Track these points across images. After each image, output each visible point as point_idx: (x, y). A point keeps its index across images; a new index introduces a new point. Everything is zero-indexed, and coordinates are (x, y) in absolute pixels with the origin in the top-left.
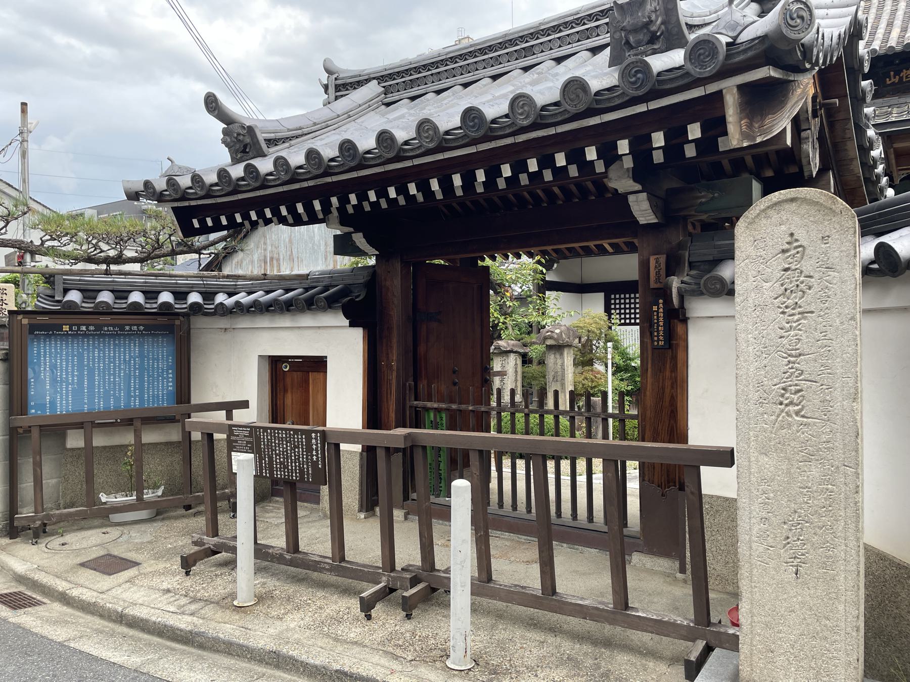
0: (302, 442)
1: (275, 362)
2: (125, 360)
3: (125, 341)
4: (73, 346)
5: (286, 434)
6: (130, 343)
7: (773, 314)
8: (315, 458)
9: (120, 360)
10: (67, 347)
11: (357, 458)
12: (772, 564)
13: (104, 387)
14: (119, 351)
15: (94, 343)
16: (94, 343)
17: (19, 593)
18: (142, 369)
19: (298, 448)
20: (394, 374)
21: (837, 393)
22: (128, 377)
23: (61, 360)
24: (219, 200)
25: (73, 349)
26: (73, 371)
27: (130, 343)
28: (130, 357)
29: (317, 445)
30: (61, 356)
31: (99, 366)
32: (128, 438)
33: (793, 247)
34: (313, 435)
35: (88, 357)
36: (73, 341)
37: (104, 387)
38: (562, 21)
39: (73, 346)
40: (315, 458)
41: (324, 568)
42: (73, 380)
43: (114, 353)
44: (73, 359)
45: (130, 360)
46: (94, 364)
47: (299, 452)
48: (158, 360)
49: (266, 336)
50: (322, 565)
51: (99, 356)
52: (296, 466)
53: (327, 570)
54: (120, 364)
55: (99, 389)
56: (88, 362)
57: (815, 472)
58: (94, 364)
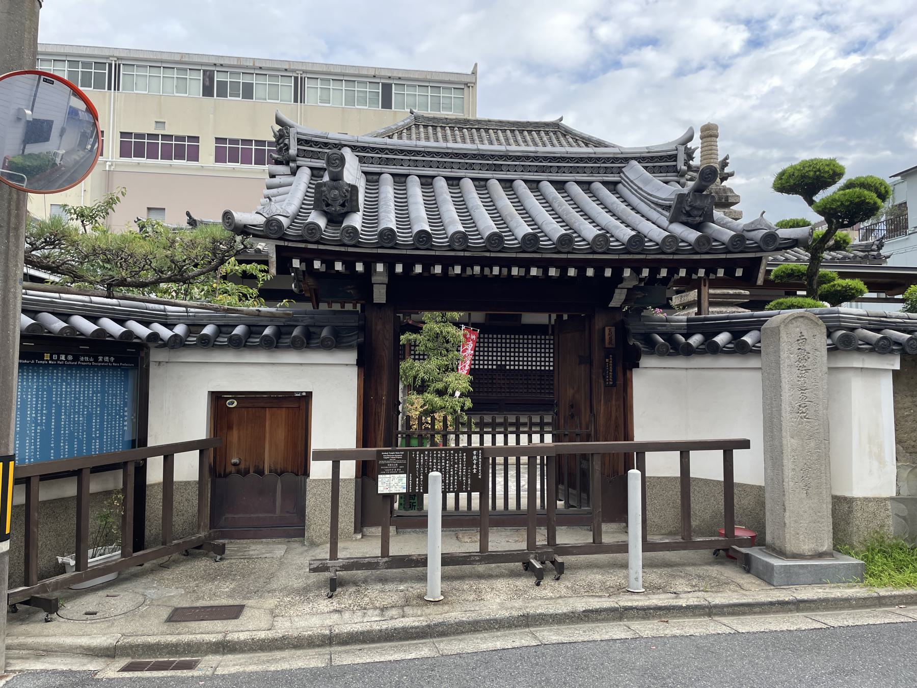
0: (462, 459)
1: (217, 398)
2: (88, 396)
3: (89, 374)
4: (43, 379)
5: (446, 454)
6: (93, 376)
7: (795, 370)
8: (475, 471)
9: (84, 397)
10: (38, 379)
11: (353, 485)
12: (797, 491)
13: (70, 427)
14: (84, 385)
15: (62, 376)
16: (62, 376)
17: (132, 663)
18: (103, 406)
19: (458, 464)
20: (384, 407)
21: (820, 407)
22: (89, 417)
23: (32, 395)
24: (290, 244)
25: (43, 382)
26: (42, 410)
27: (93, 376)
28: (93, 392)
29: (478, 460)
30: (32, 392)
31: (66, 403)
32: (69, 489)
33: (802, 339)
34: (475, 452)
35: (57, 391)
36: (43, 373)
37: (70, 427)
38: (525, 154)
39: (43, 379)
40: (475, 471)
41: (475, 561)
42: (42, 420)
43: (80, 388)
44: (42, 395)
45: (93, 397)
46: (61, 400)
47: (458, 467)
48: (116, 396)
49: (220, 371)
50: (472, 558)
51: (66, 391)
52: (454, 479)
53: (478, 561)
54: (84, 400)
55: (65, 430)
56: (56, 398)
57: (813, 444)
58: (61, 400)
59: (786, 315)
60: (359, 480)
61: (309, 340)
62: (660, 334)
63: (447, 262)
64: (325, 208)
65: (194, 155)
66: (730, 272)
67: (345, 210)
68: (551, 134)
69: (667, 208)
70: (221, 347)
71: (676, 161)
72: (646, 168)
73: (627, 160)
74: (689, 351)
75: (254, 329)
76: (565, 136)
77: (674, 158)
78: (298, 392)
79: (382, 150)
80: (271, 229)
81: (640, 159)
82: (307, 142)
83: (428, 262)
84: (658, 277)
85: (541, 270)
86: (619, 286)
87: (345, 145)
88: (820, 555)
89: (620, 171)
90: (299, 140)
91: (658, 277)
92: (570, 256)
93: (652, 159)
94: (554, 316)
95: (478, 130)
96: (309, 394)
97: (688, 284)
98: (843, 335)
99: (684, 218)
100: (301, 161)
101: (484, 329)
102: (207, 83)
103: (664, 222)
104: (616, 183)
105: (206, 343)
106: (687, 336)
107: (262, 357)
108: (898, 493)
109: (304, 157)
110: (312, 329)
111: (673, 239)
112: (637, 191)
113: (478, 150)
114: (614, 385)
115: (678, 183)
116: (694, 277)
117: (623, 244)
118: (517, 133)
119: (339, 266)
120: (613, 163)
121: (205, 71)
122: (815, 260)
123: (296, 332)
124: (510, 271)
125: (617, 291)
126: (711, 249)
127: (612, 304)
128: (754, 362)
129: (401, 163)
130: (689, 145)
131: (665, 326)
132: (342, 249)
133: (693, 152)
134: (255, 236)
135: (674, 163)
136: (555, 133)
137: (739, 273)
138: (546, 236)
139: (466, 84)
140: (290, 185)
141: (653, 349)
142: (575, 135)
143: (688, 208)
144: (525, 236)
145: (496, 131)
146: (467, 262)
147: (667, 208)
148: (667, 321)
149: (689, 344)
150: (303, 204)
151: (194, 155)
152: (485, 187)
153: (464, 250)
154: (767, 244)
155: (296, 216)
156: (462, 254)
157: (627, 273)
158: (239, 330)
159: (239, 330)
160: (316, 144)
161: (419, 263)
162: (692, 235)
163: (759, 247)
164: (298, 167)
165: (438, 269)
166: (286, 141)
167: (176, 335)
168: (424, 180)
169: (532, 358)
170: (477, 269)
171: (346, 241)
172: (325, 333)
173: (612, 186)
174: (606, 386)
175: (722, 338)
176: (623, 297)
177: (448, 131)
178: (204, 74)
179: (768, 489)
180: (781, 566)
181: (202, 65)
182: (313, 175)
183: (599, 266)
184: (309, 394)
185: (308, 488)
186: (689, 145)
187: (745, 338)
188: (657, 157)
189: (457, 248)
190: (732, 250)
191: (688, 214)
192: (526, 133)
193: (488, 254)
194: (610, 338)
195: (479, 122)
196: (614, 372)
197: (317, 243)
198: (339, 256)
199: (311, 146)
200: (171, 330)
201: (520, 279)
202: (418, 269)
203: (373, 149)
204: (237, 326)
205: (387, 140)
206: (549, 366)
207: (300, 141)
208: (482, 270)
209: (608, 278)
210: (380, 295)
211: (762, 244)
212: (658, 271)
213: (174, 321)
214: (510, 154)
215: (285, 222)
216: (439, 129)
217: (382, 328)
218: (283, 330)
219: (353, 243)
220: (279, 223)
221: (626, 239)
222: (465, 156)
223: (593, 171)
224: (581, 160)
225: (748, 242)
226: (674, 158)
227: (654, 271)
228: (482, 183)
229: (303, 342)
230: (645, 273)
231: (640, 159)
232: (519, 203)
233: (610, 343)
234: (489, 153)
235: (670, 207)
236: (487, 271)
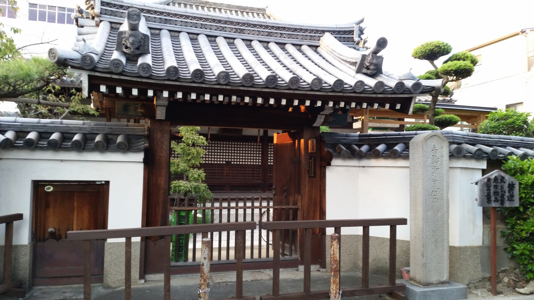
1: (38, 186)
33: (434, 149)
59: (427, 134)
60: (144, 243)
61: (108, 145)
62: (343, 144)
63: (214, 93)
64: (125, 50)
66: (392, 107)
67: (138, 52)
69: (354, 64)
70: (42, 149)
71: (353, 34)
73: (323, 32)
74: (360, 156)
75: (66, 135)
77: (351, 32)
78: (99, 181)
79: (162, 13)
80: (85, 63)
81: (333, 32)
83: (201, 92)
84: (315, 106)
85: (251, 99)
86: (321, 113)
88: (443, 283)
91: (315, 106)
92: (296, 92)
93: (339, 32)
94: (262, 131)
96: (107, 183)
97: (359, 111)
98: (456, 148)
99: (365, 71)
101: (212, 138)
103: (353, 73)
105: (31, 145)
106: (360, 146)
107: (73, 155)
108: (483, 243)
109: (105, 14)
110: (110, 137)
111: (361, 83)
113: (229, 18)
114: (314, 177)
116: (337, 107)
117: (309, 84)
119: (260, 101)
120: (315, 33)
122: (435, 100)
123: (98, 138)
124: (230, 98)
125: (319, 116)
126: (321, 88)
128: (401, 163)
129: (175, 23)
130: (362, 25)
131: (345, 139)
132: (139, 80)
133: (363, 30)
134: (73, 67)
135: (352, 36)
137: (398, 107)
140: (96, 33)
141: (340, 155)
143: (368, 64)
146: (228, 94)
147: (354, 64)
148: (347, 136)
149: (361, 151)
150: (106, 47)
153: (226, 85)
154: (416, 90)
155: (103, 55)
156: (224, 87)
158: (55, 136)
159: (55, 136)
161: (194, 92)
163: (410, 91)
164: (101, 21)
165: (207, 97)
167: (7, 139)
169: (248, 157)
170: (207, 97)
171: (142, 74)
172: (120, 139)
173: (315, 48)
174: (310, 177)
175: (381, 147)
176: (322, 120)
179: (412, 244)
180: (421, 292)
182: (112, 28)
184: (107, 183)
185: (106, 249)
186: (362, 25)
187: (395, 148)
189: (222, 83)
190: (396, 92)
191: (368, 68)
193: (242, 88)
194: (313, 147)
195: (215, 4)
197: (120, 74)
198: (135, 84)
199: (111, 7)
200: (3, 135)
201: (237, 104)
202: (180, 95)
203: (156, 12)
204: (53, 133)
205: (167, 7)
206: (259, 162)
208: (211, 98)
209: (284, 105)
210: (161, 114)
211: (412, 90)
212: (341, 102)
214: (250, 22)
215: (96, 58)
217: (161, 137)
218: (89, 136)
219: (147, 75)
220: (91, 59)
221: (310, 81)
222: (220, 21)
225: (345, 86)
226: (351, 32)
227: (313, 103)
228: (213, 39)
229: (104, 146)
231: (333, 32)
232: (239, 56)
233: (313, 149)
234: (236, 21)
235: (356, 63)
236: (214, 98)
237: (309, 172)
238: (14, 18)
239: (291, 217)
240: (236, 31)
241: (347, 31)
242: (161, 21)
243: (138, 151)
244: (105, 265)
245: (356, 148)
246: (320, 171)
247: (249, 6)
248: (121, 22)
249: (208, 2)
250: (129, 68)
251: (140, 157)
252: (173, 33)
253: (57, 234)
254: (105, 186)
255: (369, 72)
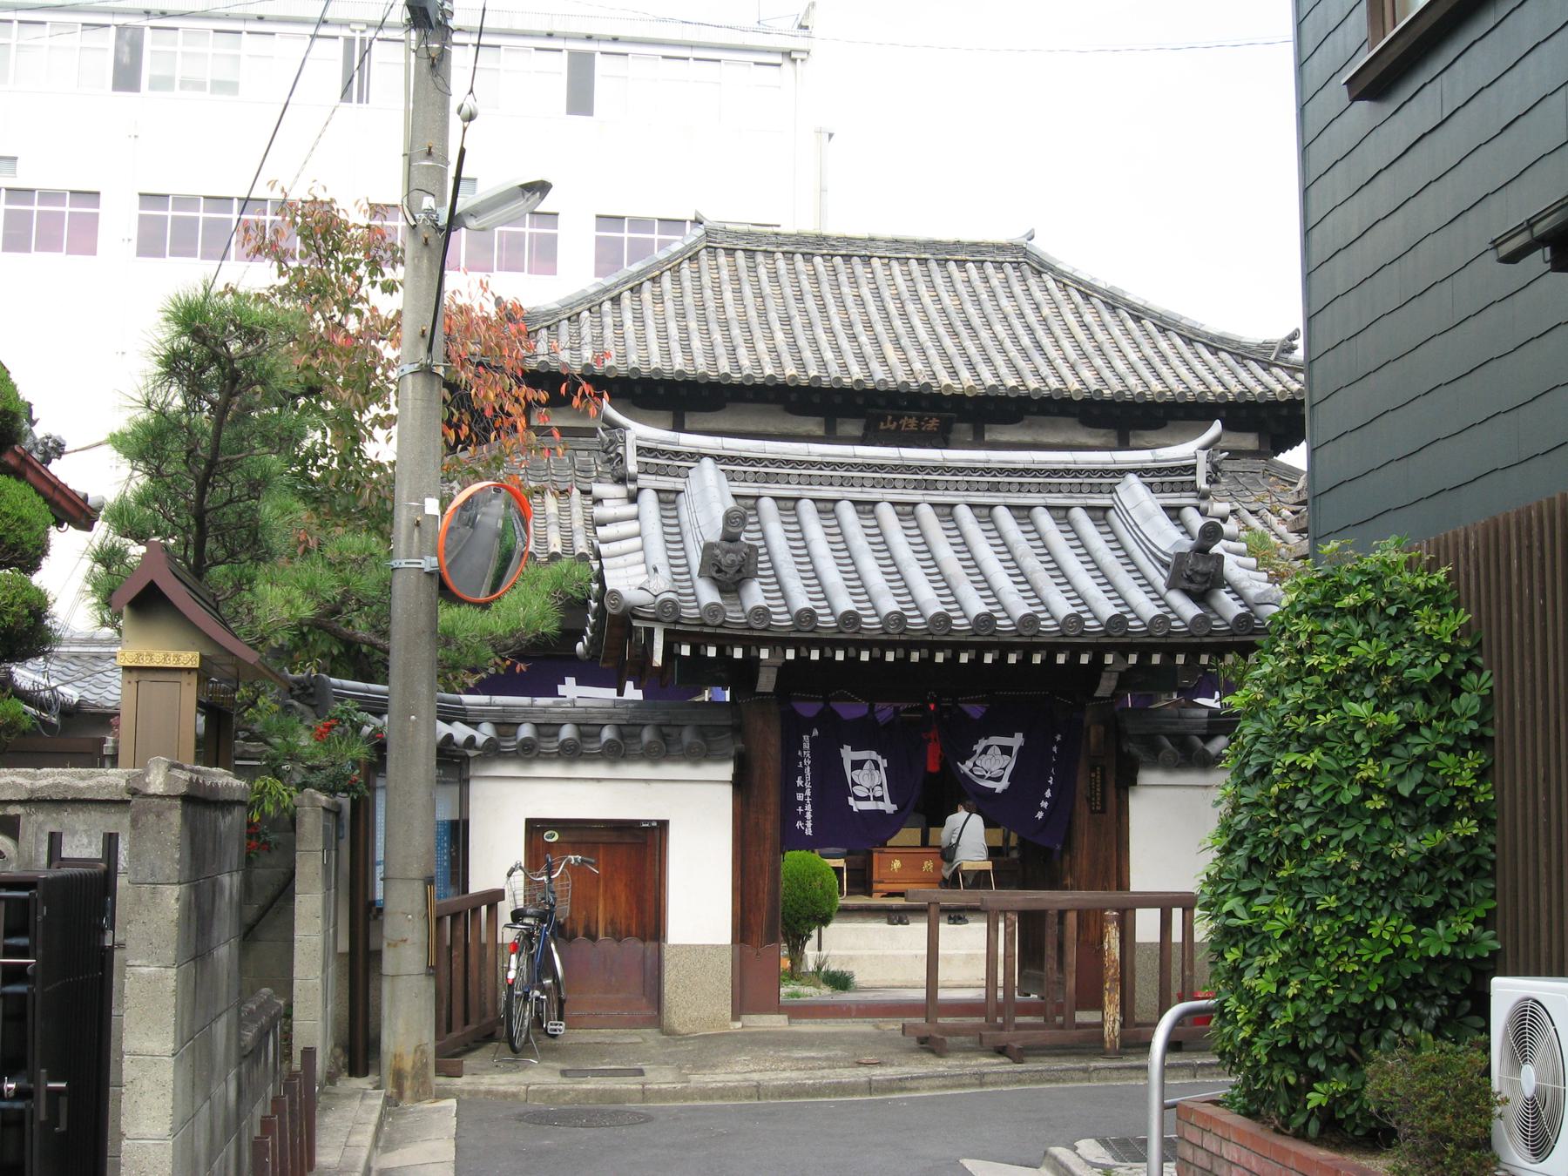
1: (535, 827)
11: (728, 954)
61: (665, 749)
62: (1167, 736)
65: (84, 238)
68: (1008, 268)
70: (548, 758)
71: (1194, 474)
72: (1150, 485)
75: (626, 730)
76: (1040, 273)
77: (1191, 469)
82: (650, 451)
87: (706, 455)
89: (1112, 490)
90: (639, 448)
95: (847, 258)
96: (663, 825)
99: (1186, 585)
100: (644, 480)
102: (126, 59)
104: (1106, 509)
106: (1208, 738)
110: (666, 730)
112: (1134, 528)
113: (901, 458)
114: (1103, 811)
115: (1197, 508)
118: (933, 265)
121: (121, 29)
127: (1098, 694)
136: (1017, 266)
138: (1003, 610)
139: (787, 54)
141: (1158, 761)
142: (1062, 274)
144: (978, 616)
145: (887, 261)
151: (84, 238)
152: (913, 515)
157: (1109, 659)
158: (567, 732)
160: (663, 453)
162: (1190, 610)
164: (639, 489)
166: (620, 450)
168: (821, 505)
173: (1099, 514)
174: (1092, 812)
176: (1113, 683)
177: (781, 264)
178: (119, 37)
181: (114, 12)
183: (1075, 650)
184: (663, 825)
188: (1166, 469)
191: (1190, 579)
192: (952, 266)
195: (849, 241)
196: (1103, 792)
207: (640, 450)
213: (478, 719)
216: (760, 258)
223: (1071, 490)
224: (1054, 472)
230: (1133, 659)
232: (963, 545)
237: (1089, 800)
238: (92, 251)
239: (1072, 918)
240: (918, 485)
241: (1178, 468)
242: (757, 478)
243: (719, 758)
244: (667, 988)
245: (1199, 742)
246: (1118, 796)
247: (967, 237)
248: (680, 487)
249: (825, 238)
250: (734, 615)
251: (726, 771)
252: (782, 504)
253: (568, 927)
254: (657, 833)
255: (1193, 587)
